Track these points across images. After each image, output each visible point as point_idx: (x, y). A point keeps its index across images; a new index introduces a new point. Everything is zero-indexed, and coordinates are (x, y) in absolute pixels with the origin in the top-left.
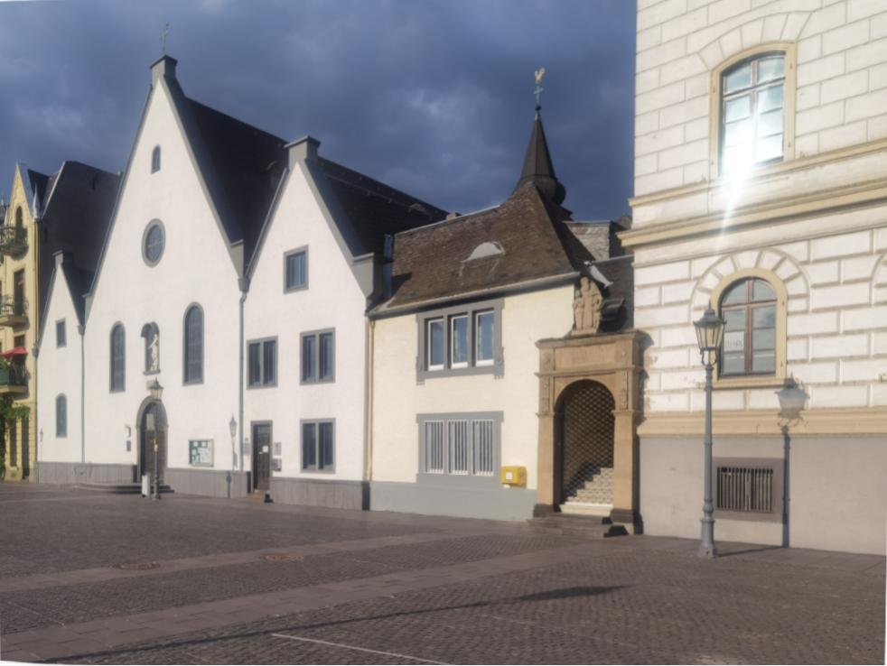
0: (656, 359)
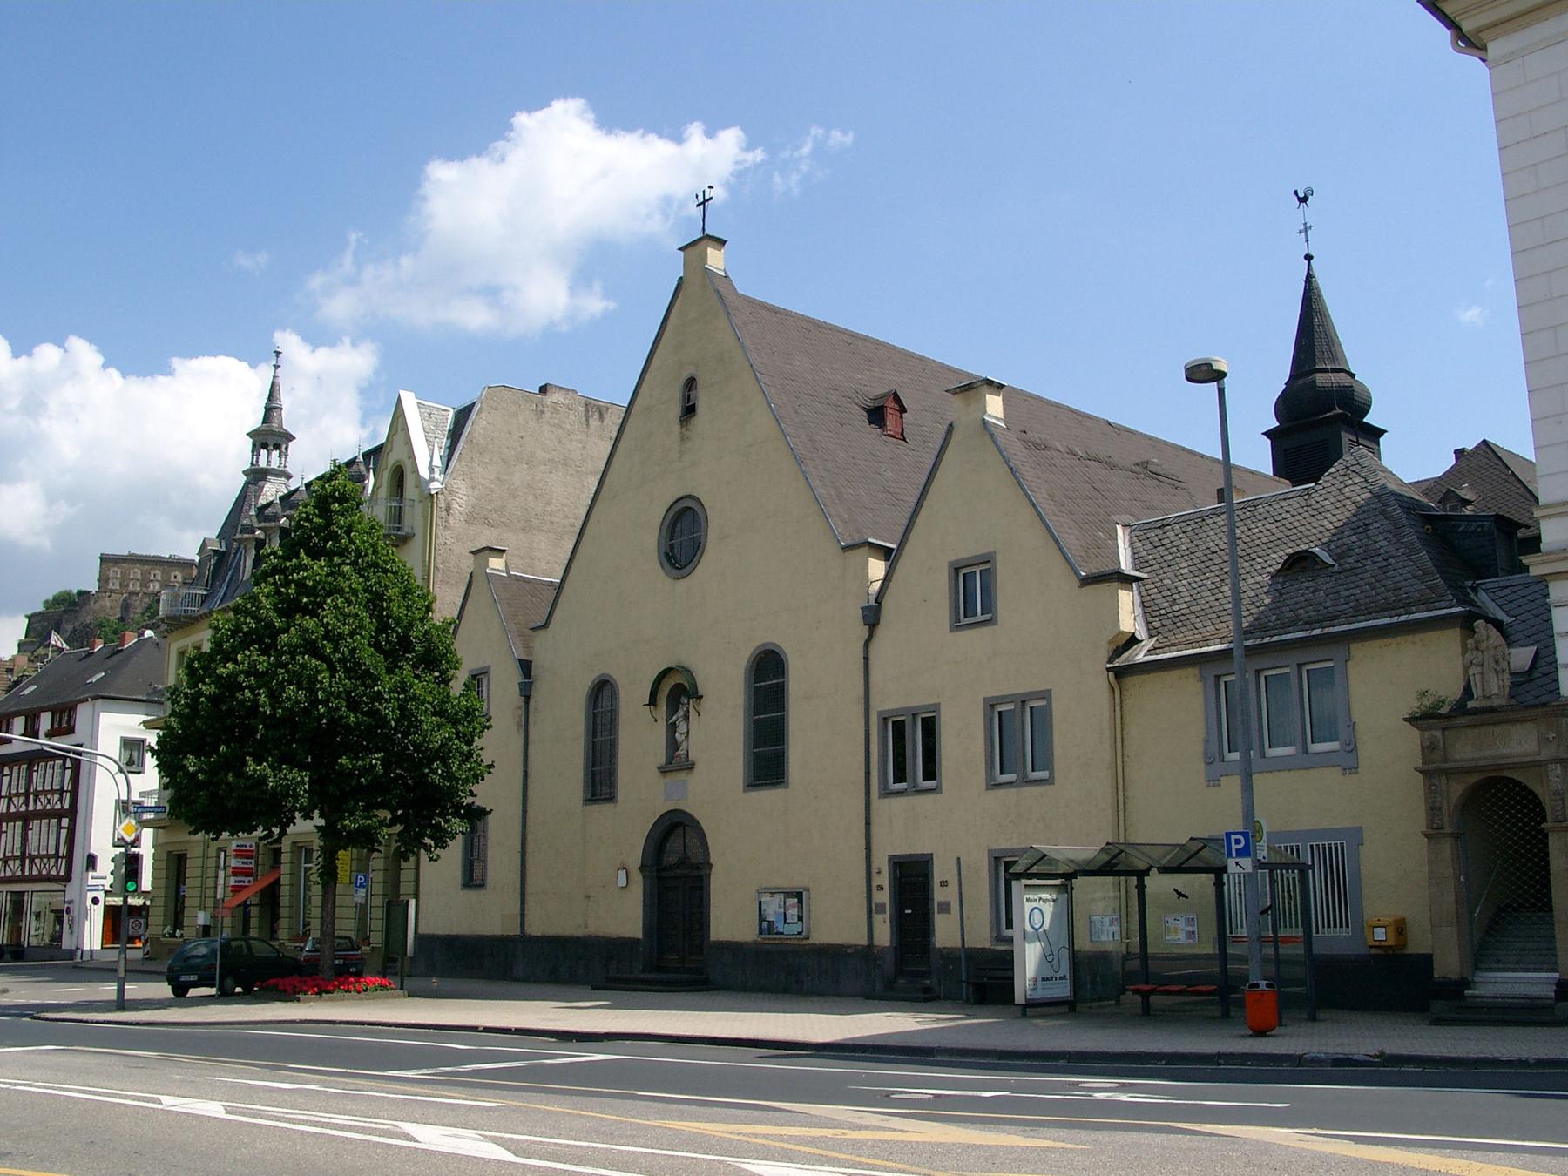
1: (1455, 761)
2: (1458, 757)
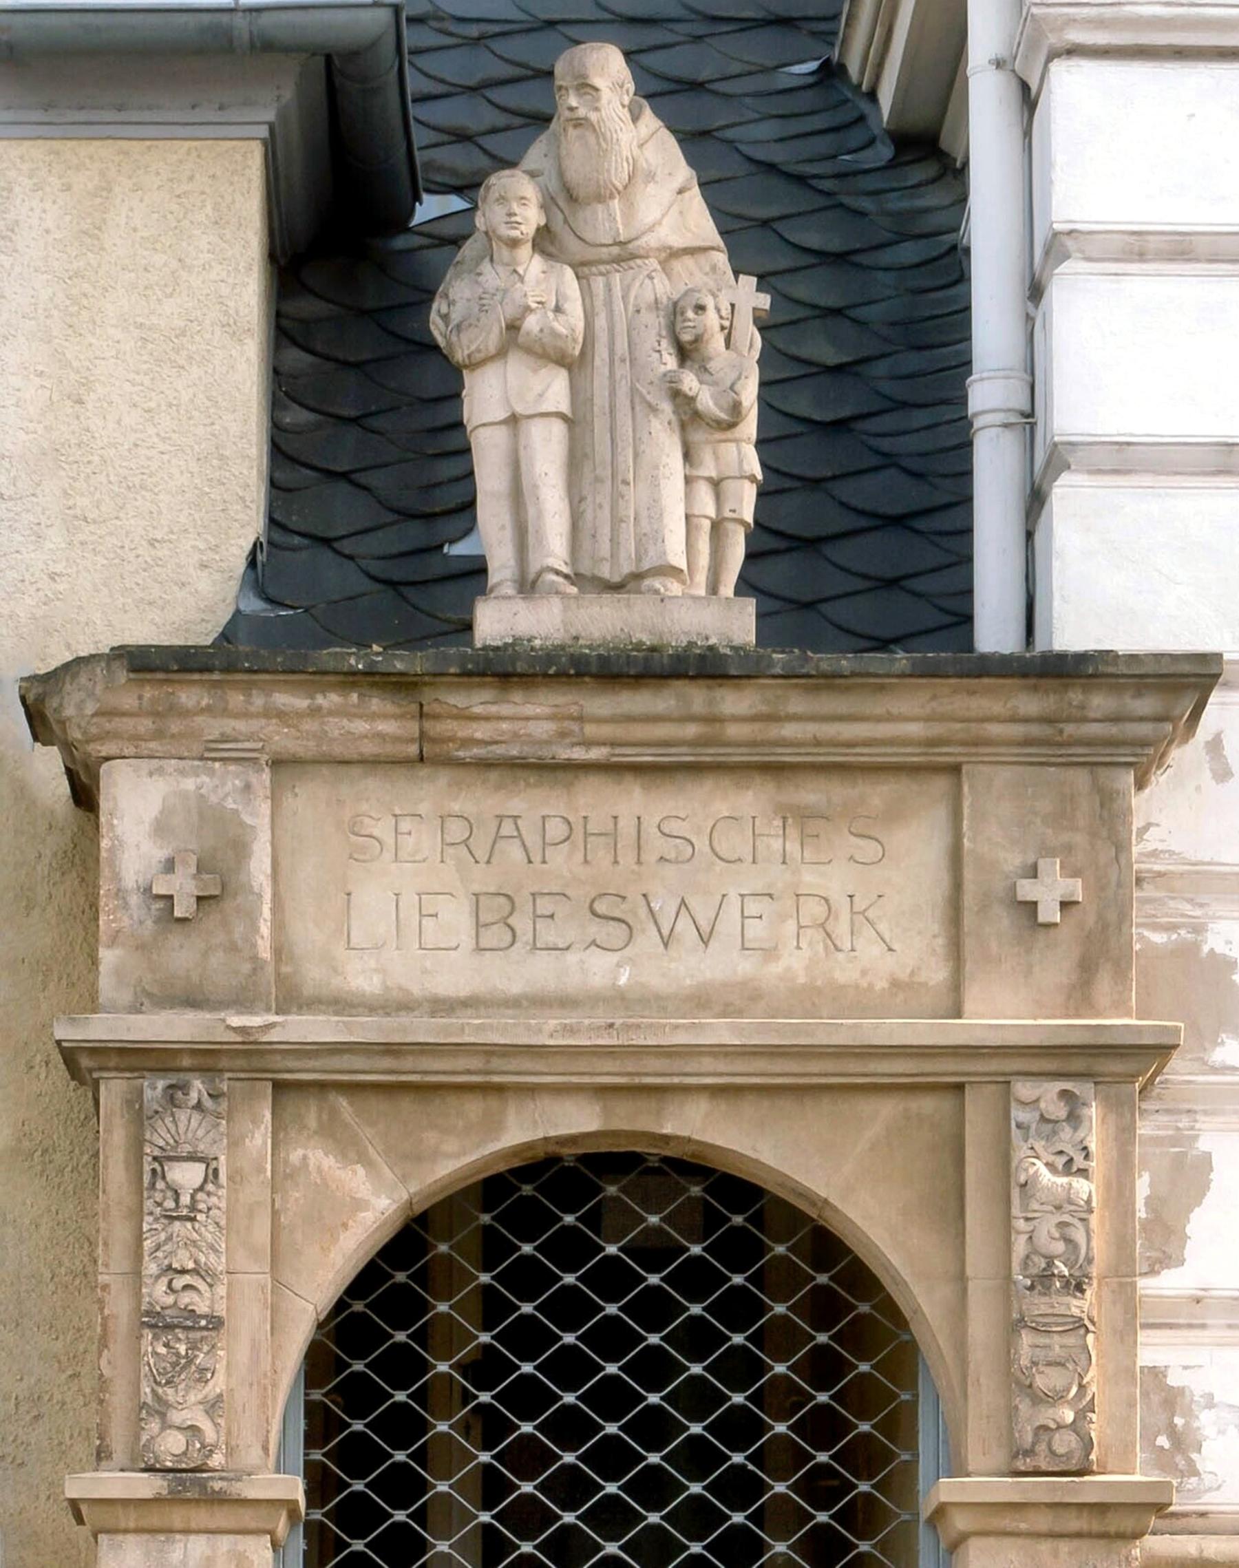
1: (341, 1004)
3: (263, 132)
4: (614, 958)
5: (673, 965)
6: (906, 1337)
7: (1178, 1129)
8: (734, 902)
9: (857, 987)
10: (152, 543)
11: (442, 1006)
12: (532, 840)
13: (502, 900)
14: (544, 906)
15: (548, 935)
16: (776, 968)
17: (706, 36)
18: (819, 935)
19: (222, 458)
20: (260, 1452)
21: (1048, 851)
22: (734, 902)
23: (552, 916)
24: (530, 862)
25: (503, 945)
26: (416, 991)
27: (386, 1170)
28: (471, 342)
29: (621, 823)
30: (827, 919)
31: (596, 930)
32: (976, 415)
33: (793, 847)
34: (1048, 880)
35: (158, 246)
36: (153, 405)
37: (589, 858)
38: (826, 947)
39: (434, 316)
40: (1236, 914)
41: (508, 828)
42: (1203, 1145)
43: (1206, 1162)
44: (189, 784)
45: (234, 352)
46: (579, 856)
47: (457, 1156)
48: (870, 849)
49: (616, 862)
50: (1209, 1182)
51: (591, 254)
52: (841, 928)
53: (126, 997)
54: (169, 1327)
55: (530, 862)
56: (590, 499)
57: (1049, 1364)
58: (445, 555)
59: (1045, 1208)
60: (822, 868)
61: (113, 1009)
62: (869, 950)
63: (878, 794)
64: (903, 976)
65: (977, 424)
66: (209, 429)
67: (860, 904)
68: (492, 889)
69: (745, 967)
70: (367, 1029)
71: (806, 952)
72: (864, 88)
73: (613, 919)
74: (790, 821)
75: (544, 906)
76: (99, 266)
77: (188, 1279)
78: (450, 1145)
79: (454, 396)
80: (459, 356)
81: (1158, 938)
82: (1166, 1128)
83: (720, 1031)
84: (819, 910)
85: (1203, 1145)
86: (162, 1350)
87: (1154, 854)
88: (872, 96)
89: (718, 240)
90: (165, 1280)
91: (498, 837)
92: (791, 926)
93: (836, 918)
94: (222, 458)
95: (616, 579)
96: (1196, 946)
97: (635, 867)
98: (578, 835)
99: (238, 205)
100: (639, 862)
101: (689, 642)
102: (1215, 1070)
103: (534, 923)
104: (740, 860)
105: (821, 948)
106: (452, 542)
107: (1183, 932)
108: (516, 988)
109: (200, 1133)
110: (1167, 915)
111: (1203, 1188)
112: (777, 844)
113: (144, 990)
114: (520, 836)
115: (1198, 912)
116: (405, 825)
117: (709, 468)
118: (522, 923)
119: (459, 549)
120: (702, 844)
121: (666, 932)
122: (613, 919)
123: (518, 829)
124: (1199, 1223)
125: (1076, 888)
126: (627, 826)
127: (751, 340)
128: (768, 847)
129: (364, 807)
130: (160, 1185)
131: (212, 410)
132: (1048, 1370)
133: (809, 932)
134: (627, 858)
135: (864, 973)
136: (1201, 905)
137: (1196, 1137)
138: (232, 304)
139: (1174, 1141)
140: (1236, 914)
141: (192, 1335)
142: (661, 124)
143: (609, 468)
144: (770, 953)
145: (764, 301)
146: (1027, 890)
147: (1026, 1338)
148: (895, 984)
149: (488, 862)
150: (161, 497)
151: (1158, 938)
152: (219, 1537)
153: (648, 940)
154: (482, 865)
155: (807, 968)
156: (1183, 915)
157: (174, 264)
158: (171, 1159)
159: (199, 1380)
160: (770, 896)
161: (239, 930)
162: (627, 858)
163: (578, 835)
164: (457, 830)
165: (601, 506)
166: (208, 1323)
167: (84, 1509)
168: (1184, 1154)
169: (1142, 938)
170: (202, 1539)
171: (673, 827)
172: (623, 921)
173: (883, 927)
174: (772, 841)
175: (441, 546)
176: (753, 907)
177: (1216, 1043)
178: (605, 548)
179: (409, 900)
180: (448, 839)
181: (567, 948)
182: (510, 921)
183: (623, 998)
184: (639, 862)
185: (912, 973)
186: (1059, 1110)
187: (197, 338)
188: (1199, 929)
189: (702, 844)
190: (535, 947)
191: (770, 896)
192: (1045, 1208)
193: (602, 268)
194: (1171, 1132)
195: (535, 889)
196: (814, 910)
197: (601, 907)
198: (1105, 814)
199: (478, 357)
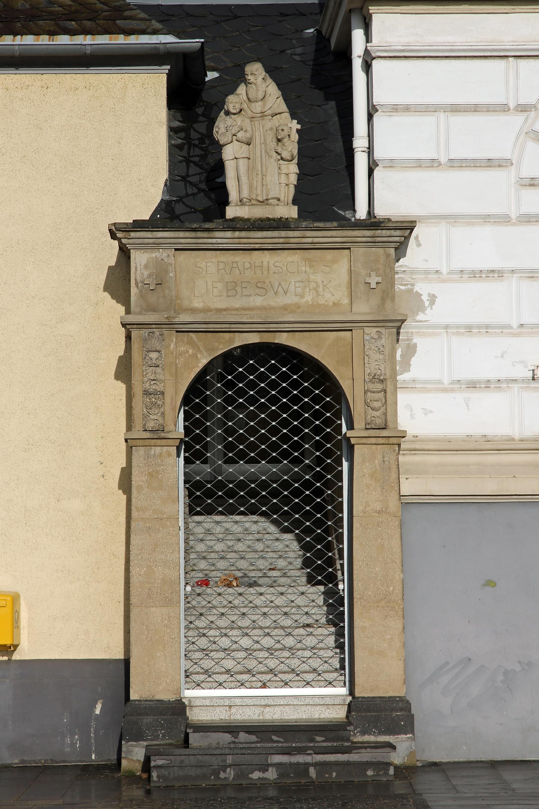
0: (433, 299)
1: (193, 311)
2: (197, 304)
3: (167, 71)
4: (263, 298)
5: (277, 300)
6: (338, 391)
7: (408, 337)
8: (293, 283)
9: (324, 305)
10: (139, 180)
11: (219, 311)
12: (241, 268)
13: (234, 284)
14: (244, 285)
15: (245, 292)
16: (304, 300)
17: (283, 21)
18: (314, 292)
19: (157, 157)
20: (174, 426)
21: (372, 270)
22: (293, 283)
23: (246, 287)
24: (241, 273)
25: (234, 295)
26: (212, 307)
27: (205, 353)
28: (224, 139)
29: (264, 263)
30: (317, 287)
31: (257, 291)
32: (355, 148)
33: (308, 269)
34: (373, 277)
35: (140, 102)
36: (139, 143)
37: (256, 272)
38: (317, 294)
39: (214, 132)
40: (537, 11)
41: (235, 265)
42: (415, 341)
43: (415, 345)
44: (154, 255)
45: (160, 129)
46: (253, 272)
47: (222, 349)
48: (327, 269)
49: (263, 273)
50: (416, 350)
51: (255, 115)
52: (320, 289)
53: (138, 310)
54: (150, 394)
55: (241, 273)
56: (255, 179)
57: (375, 401)
58: (216, 182)
59: (373, 361)
60: (315, 274)
61: (135, 314)
62: (328, 295)
63: (329, 255)
64: (336, 302)
65: (355, 150)
66: (153, 150)
67: (325, 283)
68: (231, 281)
69: (296, 300)
70: (199, 318)
71: (311, 296)
72: (326, 37)
73: (262, 288)
74: (307, 262)
75: (244, 285)
76: (124, 107)
77: (154, 382)
78: (221, 346)
79: (220, 153)
80: (221, 142)
81: (403, 288)
82: (405, 336)
83: (290, 318)
84: (315, 285)
85: (415, 341)
86: (148, 400)
87: (401, 266)
88: (329, 40)
89: (287, 110)
90: (149, 382)
91: (232, 267)
92: (307, 289)
93: (319, 287)
94: (157, 157)
95: (262, 200)
96: (412, 290)
97: (267, 275)
98: (253, 267)
99: (160, 91)
100: (268, 273)
101: (281, 217)
102: (417, 322)
103: (242, 289)
104: (294, 272)
105: (315, 295)
106: (218, 177)
107: (409, 286)
108: (237, 306)
109: (157, 344)
110: (405, 281)
111: (415, 352)
112: (303, 268)
113: (142, 308)
114: (238, 267)
115: (413, 281)
116: (209, 264)
117: (284, 171)
118: (239, 289)
119: (219, 180)
120: (284, 269)
121: (275, 292)
122: (262, 288)
123: (237, 265)
124: (413, 361)
125: (379, 279)
126: (265, 264)
127: (295, 137)
128: (302, 269)
129: (198, 260)
130: (147, 358)
131: (154, 145)
132: (374, 402)
133: (312, 291)
134: (266, 273)
135: (326, 301)
136: (414, 279)
137: (412, 339)
138: (159, 117)
139: (408, 340)
140: (537, 11)
141: (156, 396)
142: (272, 80)
143: (274, 704)
144: (302, 296)
145: (299, 127)
146: (368, 280)
147: (369, 394)
148: (334, 304)
149: (230, 274)
150: (141, 167)
151: (403, 288)
152: (163, 447)
153: (271, 293)
154: (229, 275)
155: (312, 300)
156: (409, 282)
157: (144, 106)
158: (150, 351)
159: (158, 408)
160: (302, 282)
161: (167, 292)
162: (266, 273)
163: (253, 267)
164: (221, 266)
165: (258, 181)
166: (160, 393)
167: (128, 440)
168: (410, 343)
169: (398, 288)
170: (159, 447)
171: (277, 264)
172: (264, 288)
173: (331, 289)
174: (302, 267)
175: (215, 179)
176: (297, 285)
177: (418, 315)
178: (259, 192)
179: (210, 283)
180: (220, 268)
181: (250, 296)
182: (236, 289)
183: (265, 308)
184: (268, 273)
185: (339, 301)
186: (376, 336)
187: (150, 126)
188: (413, 285)
189: (284, 269)
190: (242, 296)
191: (302, 282)
192: (373, 361)
193: (257, 119)
194: (406, 338)
195: (242, 280)
196: (313, 285)
197: (259, 285)
198: (388, 260)
199: (226, 143)
